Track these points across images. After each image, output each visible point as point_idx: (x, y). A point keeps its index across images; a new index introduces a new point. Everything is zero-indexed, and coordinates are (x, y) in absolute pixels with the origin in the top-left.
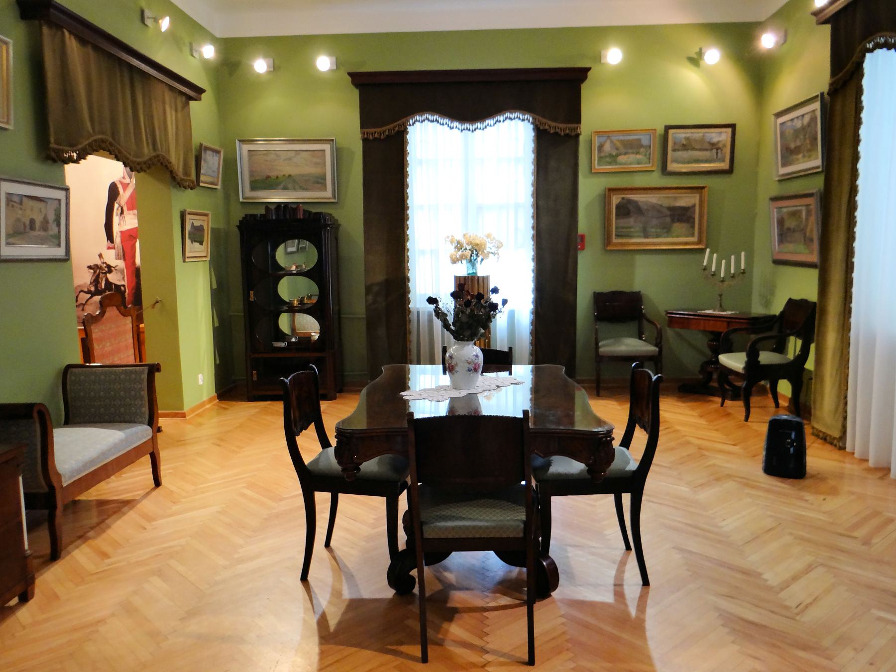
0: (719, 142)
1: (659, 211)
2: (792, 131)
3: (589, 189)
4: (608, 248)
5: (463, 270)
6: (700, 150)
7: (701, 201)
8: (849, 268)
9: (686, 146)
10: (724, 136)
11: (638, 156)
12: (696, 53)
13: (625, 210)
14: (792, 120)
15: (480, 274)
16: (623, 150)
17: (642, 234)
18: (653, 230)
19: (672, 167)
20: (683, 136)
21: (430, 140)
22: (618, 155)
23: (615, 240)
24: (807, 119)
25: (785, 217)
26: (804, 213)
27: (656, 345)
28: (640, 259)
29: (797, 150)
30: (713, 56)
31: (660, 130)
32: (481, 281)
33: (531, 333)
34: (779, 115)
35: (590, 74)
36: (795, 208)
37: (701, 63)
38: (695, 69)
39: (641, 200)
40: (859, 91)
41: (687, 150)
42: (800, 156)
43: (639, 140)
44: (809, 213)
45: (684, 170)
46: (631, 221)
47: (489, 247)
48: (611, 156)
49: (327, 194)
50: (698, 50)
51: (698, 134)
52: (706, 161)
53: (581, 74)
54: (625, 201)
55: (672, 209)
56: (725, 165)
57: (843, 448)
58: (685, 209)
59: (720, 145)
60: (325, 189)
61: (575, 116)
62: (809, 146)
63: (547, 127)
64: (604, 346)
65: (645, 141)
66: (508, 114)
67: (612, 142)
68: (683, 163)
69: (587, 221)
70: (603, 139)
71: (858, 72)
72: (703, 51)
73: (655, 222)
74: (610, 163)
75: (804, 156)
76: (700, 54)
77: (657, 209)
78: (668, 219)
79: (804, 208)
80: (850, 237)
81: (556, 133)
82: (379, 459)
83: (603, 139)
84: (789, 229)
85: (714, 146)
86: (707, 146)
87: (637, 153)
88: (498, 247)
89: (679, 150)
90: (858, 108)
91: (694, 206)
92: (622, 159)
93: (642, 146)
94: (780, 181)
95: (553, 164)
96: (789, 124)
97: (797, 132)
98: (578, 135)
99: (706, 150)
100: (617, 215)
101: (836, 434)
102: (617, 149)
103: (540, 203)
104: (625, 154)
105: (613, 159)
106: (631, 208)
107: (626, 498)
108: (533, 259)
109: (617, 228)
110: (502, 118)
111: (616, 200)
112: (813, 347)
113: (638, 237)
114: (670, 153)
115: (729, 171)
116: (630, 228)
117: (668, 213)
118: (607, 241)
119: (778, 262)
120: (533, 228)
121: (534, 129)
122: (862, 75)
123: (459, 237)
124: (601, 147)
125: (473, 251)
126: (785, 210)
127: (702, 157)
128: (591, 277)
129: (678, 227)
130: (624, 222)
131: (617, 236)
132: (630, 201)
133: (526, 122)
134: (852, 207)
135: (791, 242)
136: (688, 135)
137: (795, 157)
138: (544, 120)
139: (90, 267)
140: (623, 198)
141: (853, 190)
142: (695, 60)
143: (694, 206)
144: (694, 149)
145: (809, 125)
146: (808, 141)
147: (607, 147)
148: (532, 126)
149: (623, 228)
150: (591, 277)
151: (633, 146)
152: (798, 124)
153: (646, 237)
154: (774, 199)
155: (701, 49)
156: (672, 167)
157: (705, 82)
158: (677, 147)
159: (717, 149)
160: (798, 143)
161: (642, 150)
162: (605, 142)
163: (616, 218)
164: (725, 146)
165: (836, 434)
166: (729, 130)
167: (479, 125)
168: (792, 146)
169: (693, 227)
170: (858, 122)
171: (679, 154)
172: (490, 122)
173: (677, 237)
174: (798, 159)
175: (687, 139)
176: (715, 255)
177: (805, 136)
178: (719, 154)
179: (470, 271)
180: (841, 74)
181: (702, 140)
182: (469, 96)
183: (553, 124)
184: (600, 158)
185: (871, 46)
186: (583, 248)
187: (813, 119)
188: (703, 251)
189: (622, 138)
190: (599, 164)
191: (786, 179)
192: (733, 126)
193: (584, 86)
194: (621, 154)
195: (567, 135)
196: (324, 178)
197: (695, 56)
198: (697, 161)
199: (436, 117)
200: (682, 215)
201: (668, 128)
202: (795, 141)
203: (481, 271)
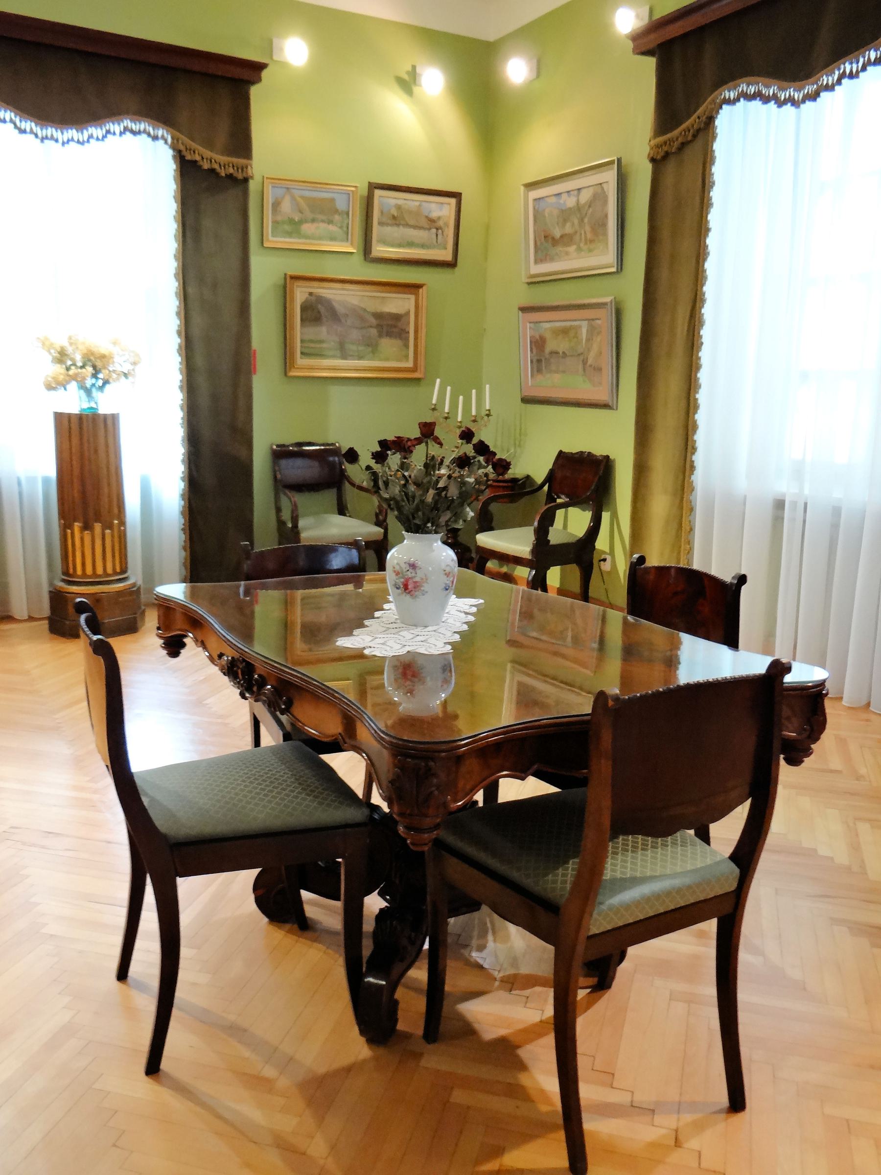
0: (439, 218)
1: (362, 319)
2: (556, 212)
3: (265, 273)
4: (292, 374)
5: (73, 402)
6: (415, 227)
7: (417, 307)
8: (689, 406)
9: (396, 220)
10: (444, 210)
11: (331, 228)
12: (408, 73)
13: (314, 312)
14: (559, 195)
15: (104, 409)
16: (309, 215)
17: (338, 353)
18: (354, 348)
19: (380, 250)
20: (393, 202)
22: (301, 222)
23: (300, 361)
24: (585, 196)
25: (548, 335)
26: (584, 331)
27: (378, 523)
28: (335, 391)
29: (566, 240)
30: (434, 80)
31: (364, 191)
32: (109, 422)
33: (182, 513)
34: (531, 186)
35: (265, 74)
36: (568, 324)
37: (416, 89)
38: (405, 96)
39: (338, 298)
40: (707, 159)
41: (398, 225)
42: (572, 249)
43: (332, 200)
44: (592, 330)
45: (393, 256)
46: (322, 331)
47: (120, 364)
48: (291, 221)
50: (410, 69)
52: (423, 246)
53: (255, 69)
54: (313, 298)
55: (378, 316)
58: (397, 317)
59: (441, 223)
61: (241, 144)
62: (589, 236)
63: (198, 158)
64: (306, 529)
65: (341, 205)
66: (127, 123)
67: (293, 198)
68: (392, 246)
70: (280, 192)
71: (706, 129)
72: (418, 70)
73: (355, 334)
74: (289, 234)
75: (579, 249)
76: (414, 74)
77: (359, 314)
78: (374, 332)
79: (585, 324)
80: (692, 366)
81: (212, 171)
82: (264, 725)
83: (280, 192)
84: (554, 353)
85: (432, 223)
86: (424, 223)
87: (330, 222)
88: (135, 364)
89: (387, 225)
90: (705, 183)
91: (408, 313)
92: (307, 228)
93: (336, 211)
94: (529, 284)
95: (207, 223)
96: (553, 200)
97: (565, 215)
98: (246, 180)
99: (421, 228)
100: (302, 320)
102: (301, 212)
103: (190, 290)
104: (313, 221)
106: (322, 309)
108: (181, 388)
109: (302, 341)
110: (116, 128)
111: (300, 294)
112: (606, 516)
113: (334, 357)
114: (376, 229)
115: (452, 265)
116: (321, 342)
117: (374, 321)
118: (287, 361)
119: (526, 400)
120: (179, 333)
121: (174, 157)
122: (714, 137)
123: (61, 341)
124: (276, 205)
125: (95, 367)
126: (547, 325)
127: (415, 242)
129: (388, 345)
130: (312, 332)
132: (320, 300)
133: (161, 142)
134: (694, 321)
135: (557, 372)
136: (400, 202)
137: (560, 249)
138: (194, 145)
140: (311, 294)
141: (697, 300)
142: (407, 84)
143: (408, 313)
144: (407, 225)
145: (590, 204)
146: (588, 228)
147: (286, 206)
148: (170, 152)
149: (311, 341)
150: (274, 420)
151: (323, 210)
152: (570, 202)
153: (344, 357)
154: (524, 309)
155: (414, 67)
156: (380, 250)
157: (415, 119)
158: (384, 220)
159: (437, 229)
160: (568, 229)
161: (337, 217)
162: (283, 197)
163: (302, 325)
164: (447, 225)
166: (453, 201)
167: (72, 133)
168: (557, 233)
169: (407, 346)
170: (704, 204)
171: (388, 230)
172: (96, 131)
173: (387, 359)
174: (567, 253)
177: (582, 220)
178: (440, 237)
179: (86, 405)
180: (676, 132)
181: (417, 213)
183: (208, 154)
184: (275, 223)
185: (732, 95)
189: (307, 194)
190: (273, 236)
191: (535, 282)
193: (255, 91)
194: (306, 222)
195: (230, 177)
197: (406, 77)
200: (391, 326)
201: (373, 187)
202: (564, 225)
203: (105, 403)
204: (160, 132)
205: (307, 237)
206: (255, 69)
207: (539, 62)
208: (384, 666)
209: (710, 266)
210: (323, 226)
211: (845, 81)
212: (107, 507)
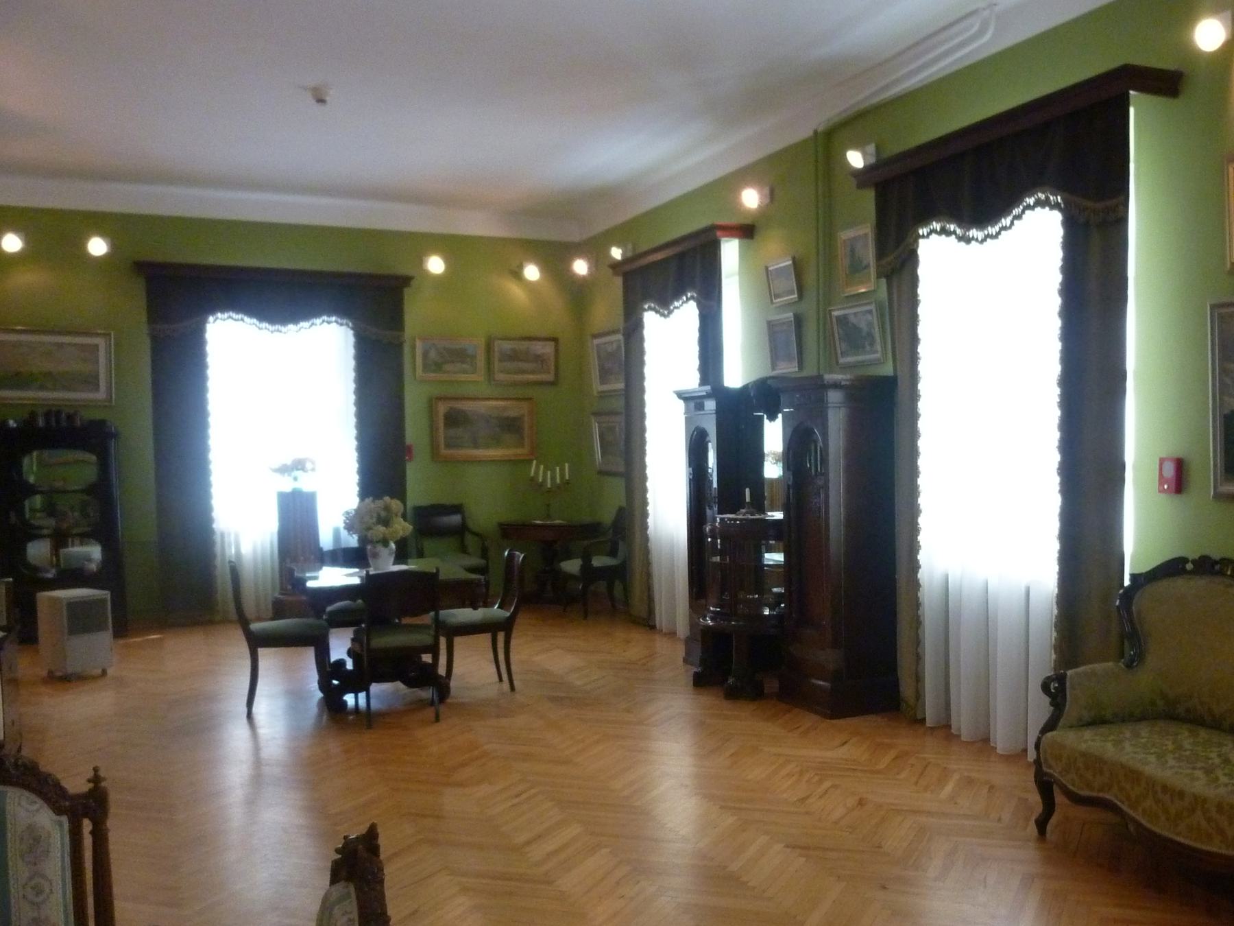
10: (547, 349)
13: (454, 419)
19: (500, 377)
21: (232, 343)
24: (615, 346)
30: (532, 272)
35: (413, 283)
47: (309, 466)
49: (101, 395)
51: (524, 345)
52: (533, 372)
53: (406, 281)
56: (550, 377)
57: (653, 627)
60: (97, 346)
66: (325, 318)
69: (415, 430)
71: (911, 259)
74: (434, 371)
85: (539, 359)
87: (463, 362)
92: (447, 367)
101: (644, 614)
105: (438, 367)
107: (87, 826)
110: (318, 321)
111: (442, 408)
128: (422, 485)
131: (448, 446)
139: (96, 779)
142: (517, 274)
165: (644, 614)
166: (553, 343)
175: (514, 350)
176: (532, 474)
182: (280, 288)
186: (410, 459)
187: (619, 347)
188: (530, 461)
192: (555, 340)
196: (97, 377)
198: (523, 372)
199: (240, 316)
204: (334, 319)
205: (448, 372)
206: (406, 281)
207: (597, 261)
208: (1084, 664)
209: (921, 349)
210: (459, 365)
211: (1016, 222)
212: (230, 595)
